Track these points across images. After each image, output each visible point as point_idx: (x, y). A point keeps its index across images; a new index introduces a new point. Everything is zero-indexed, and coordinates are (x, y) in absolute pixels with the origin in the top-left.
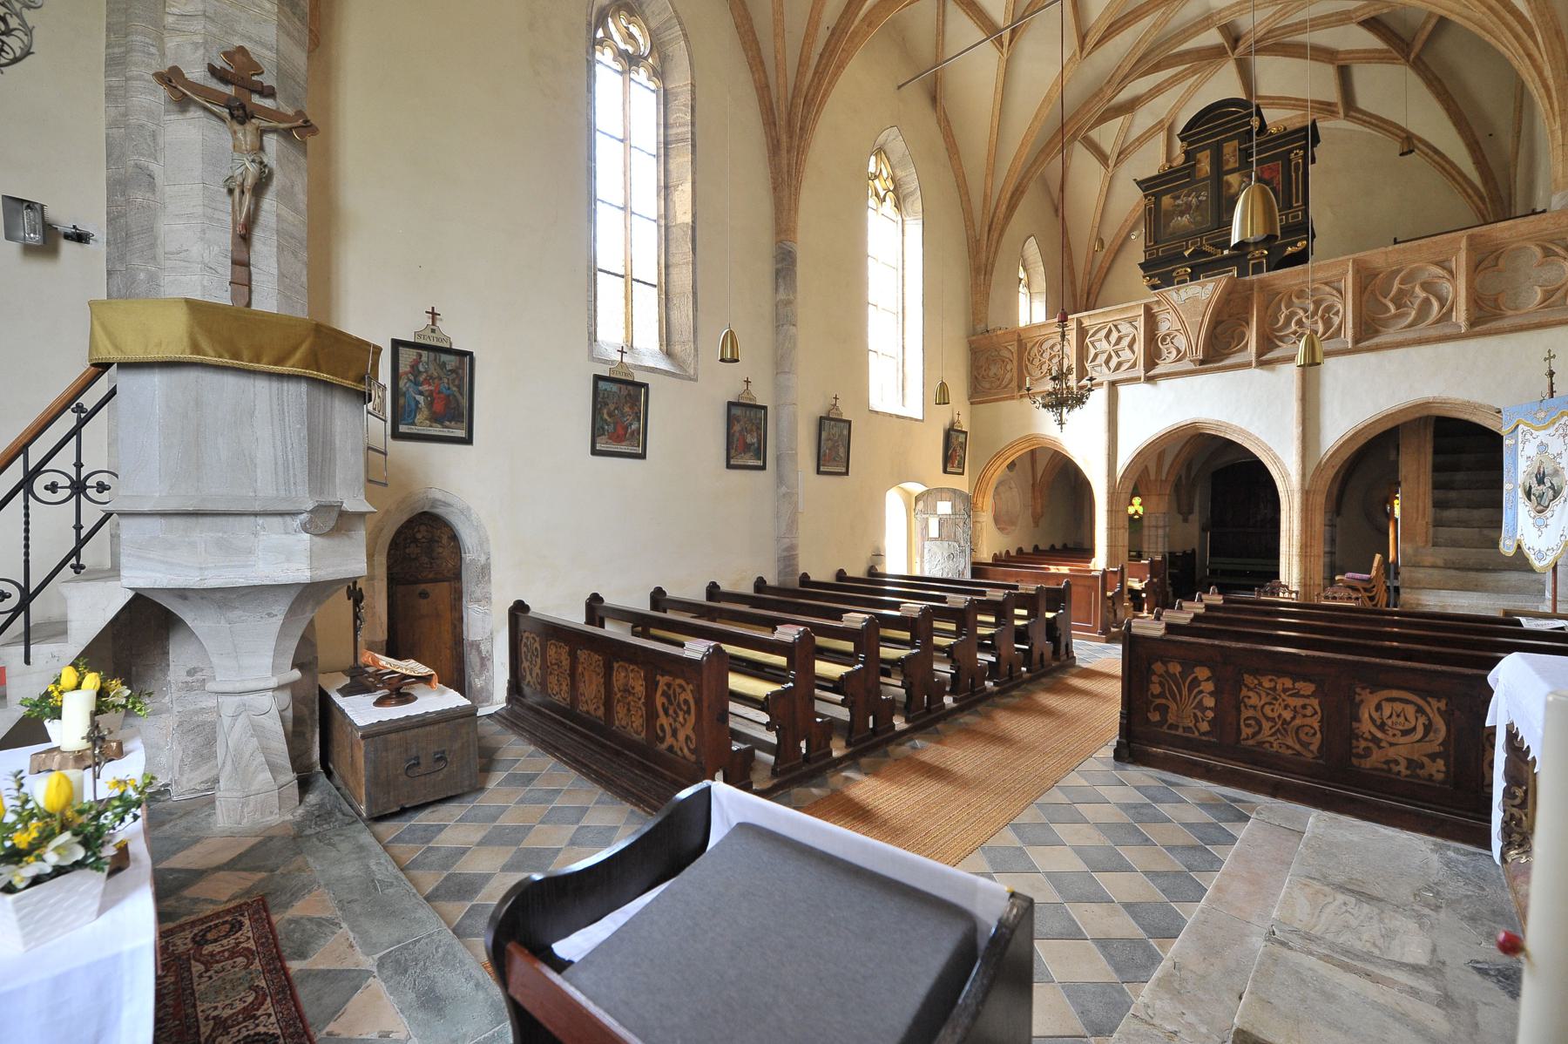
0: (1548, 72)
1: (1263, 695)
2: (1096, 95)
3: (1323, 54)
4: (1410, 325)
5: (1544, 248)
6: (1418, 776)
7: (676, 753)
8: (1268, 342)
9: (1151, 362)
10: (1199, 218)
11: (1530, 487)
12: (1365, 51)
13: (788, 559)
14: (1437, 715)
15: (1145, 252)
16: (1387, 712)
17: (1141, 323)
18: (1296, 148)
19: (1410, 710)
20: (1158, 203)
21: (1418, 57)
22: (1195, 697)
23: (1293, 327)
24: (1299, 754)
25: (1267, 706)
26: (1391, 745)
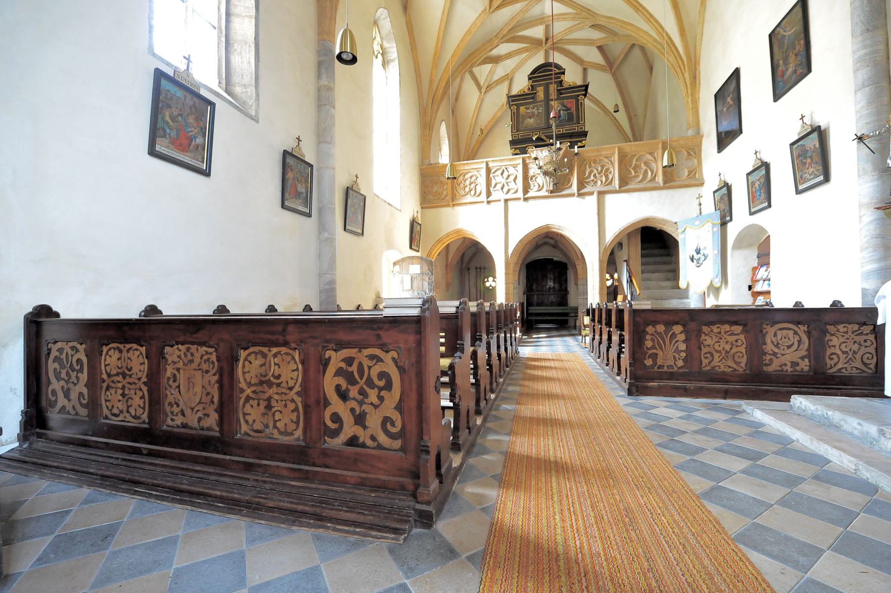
1: (714, 337)
2: (489, 41)
4: (640, 182)
5: (688, 152)
6: (796, 371)
7: (363, 445)
9: (526, 189)
10: (538, 121)
11: (693, 256)
12: (595, 64)
13: (328, 291)
14: (804, 334)
15: (512, 135)
16: (779, 337)
17: (520, 168)
18: (581, 95)
19: (791, 333)
21: (614, 72)
22: (674, 345)
23: (592, 177)
24: (735, 370)
25: (716, 344)
26: (783, 355)
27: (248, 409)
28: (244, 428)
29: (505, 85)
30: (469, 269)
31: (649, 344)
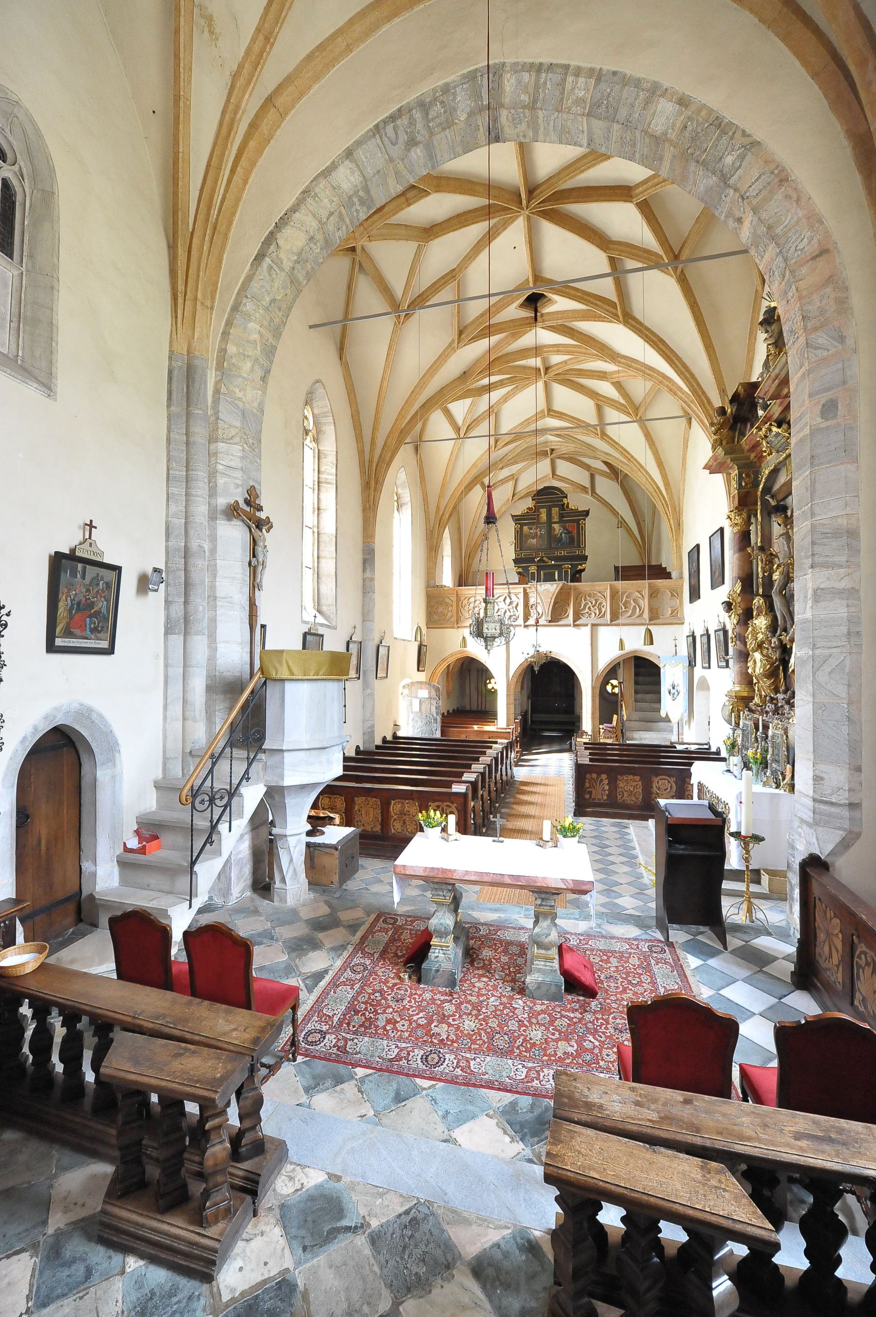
0: (672, 522)
3: (587, 467)
8: (577, 616)
17: (521, 596)
20: (521, 528)
23: (587, 610)
27: (395, 824)
28: (393, 831)
29: (511, 484)
30: (469, 671)
31: (587, 785)
